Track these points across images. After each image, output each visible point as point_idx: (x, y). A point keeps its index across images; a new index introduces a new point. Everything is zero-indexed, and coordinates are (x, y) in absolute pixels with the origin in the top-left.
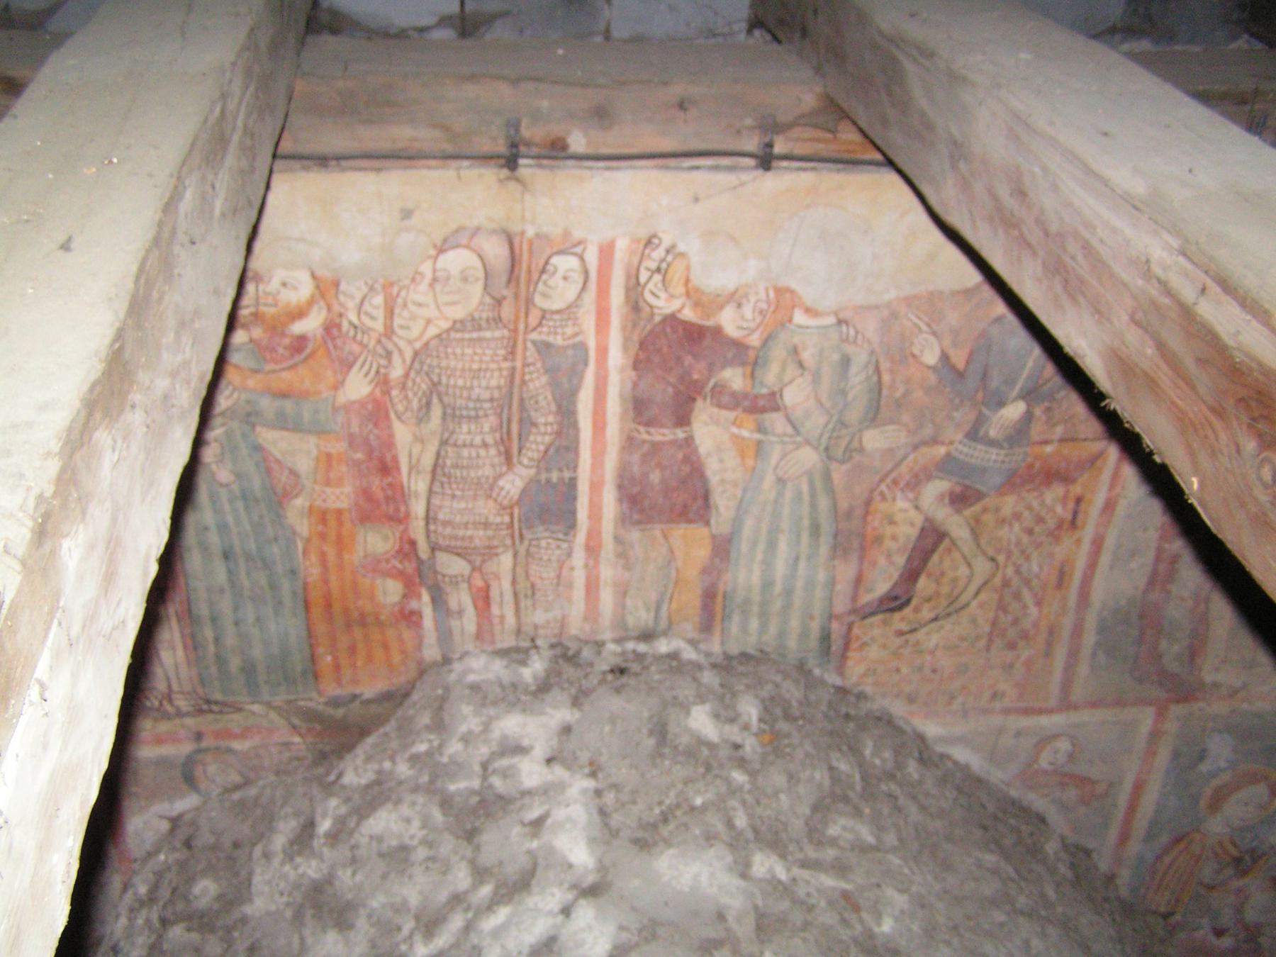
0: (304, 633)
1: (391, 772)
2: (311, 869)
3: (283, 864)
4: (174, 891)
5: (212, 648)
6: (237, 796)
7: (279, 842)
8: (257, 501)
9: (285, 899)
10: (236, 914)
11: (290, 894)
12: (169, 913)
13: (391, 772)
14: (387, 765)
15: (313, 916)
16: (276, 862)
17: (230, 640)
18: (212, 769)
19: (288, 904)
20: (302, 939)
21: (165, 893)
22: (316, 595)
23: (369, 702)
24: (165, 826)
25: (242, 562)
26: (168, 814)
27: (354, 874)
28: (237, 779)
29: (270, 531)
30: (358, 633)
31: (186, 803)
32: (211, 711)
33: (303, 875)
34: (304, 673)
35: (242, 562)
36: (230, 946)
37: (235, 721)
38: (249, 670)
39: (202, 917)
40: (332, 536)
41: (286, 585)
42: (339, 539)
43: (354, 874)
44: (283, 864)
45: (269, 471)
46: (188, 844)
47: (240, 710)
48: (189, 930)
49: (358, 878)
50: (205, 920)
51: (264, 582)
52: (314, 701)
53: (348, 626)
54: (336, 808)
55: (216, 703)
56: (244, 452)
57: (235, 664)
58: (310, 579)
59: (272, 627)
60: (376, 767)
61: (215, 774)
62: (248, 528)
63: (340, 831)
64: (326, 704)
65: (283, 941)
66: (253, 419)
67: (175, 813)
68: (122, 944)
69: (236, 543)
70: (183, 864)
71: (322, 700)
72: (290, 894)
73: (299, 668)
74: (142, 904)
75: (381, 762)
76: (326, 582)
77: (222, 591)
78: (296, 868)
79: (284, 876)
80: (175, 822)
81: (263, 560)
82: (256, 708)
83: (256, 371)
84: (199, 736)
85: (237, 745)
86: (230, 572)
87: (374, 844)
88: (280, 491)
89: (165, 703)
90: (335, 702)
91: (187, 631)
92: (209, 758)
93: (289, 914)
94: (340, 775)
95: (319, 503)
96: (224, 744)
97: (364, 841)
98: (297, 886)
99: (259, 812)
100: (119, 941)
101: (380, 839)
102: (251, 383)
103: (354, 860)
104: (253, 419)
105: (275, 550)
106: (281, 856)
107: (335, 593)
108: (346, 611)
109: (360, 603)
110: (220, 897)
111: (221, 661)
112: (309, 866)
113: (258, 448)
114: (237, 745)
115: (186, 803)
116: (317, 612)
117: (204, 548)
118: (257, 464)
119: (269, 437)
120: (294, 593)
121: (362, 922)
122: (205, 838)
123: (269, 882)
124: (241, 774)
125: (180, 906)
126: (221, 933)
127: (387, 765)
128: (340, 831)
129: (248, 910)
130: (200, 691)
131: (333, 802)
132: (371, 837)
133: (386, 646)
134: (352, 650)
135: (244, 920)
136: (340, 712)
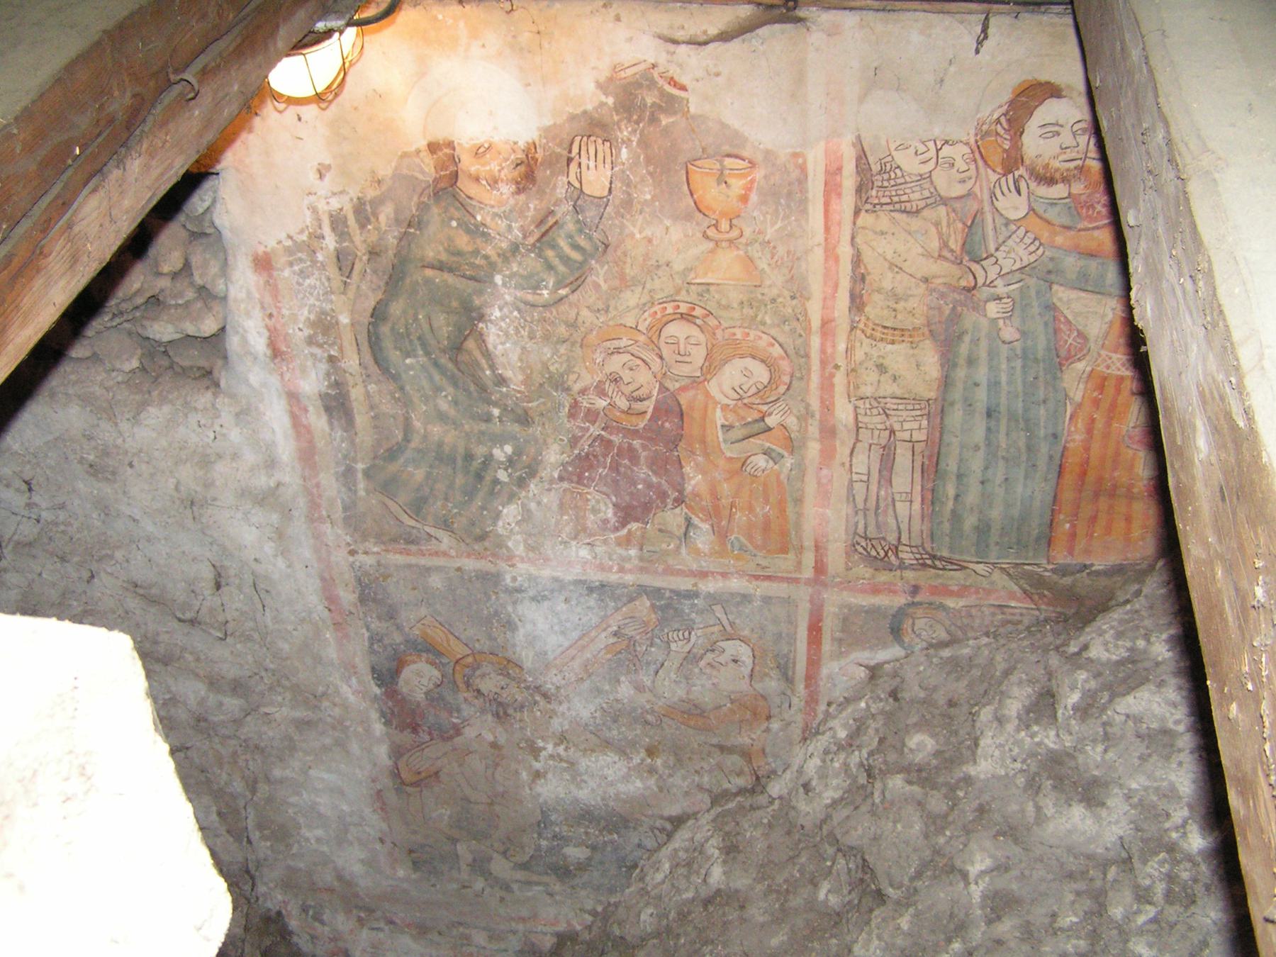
0: (1049, 498)
1: (1145, 651)
2: (1049, 739)
3: (1018, 730)
4: (881, 741)
5: (950, 504)
6: (946, 653)
7: (1013, 707)
8: (1036, 360)
9: (1018, 765)
10: (958, 773)
11: (1024, 761)
12: (878, 761)
13: (1145, 651)
14: (1141, 643)
15: (1054, 787)
16: (1010, 727)
17: (972, 497)
18: (920, 623)
19: (1022, 771)
20: (1038, 809)
21: (870, 740)
22: (1073, 461)
23: (1098, 573)
24: (862, 673)
25: (1004, 422)
26: (866, 662)
27: (1106, 751)
28: (943, 635)
29: (1041, 394)
30: (1103, 503)
31: (888, 654)
32: (935, 567)
33: (1039, 744)
34: (1038, 540)
35: (1004, 422)
36: (955, 805)
37: (955, 578)
38: (983, 530)
39: (920, 771)
40: (1105, 405)
41: (1044, 449)
42: (1113, 406)
43: (1106, 751)
44: (1018, 730)
45: (1056, 331)
46: (894, 695)
47: (963, 568)
48: (910, 783)
49: (1110, 755)
50: (924, 774)
51: (1022, 443)
52: (1043, 568)
53: (1097, 495)
54: (1086, 681)
55: (941, 559)
56: (1036, 310)
57: (970, 521)
58: (1071, 445)
59: (1020, 489)
60: (1129, 644)
61: (923, 628)
62: (1020, 389)
63: (1090, 706)
64: (1053, 571)
65: (1014, 807)
66: (1053, 277)
67: (872, 663)
68: (814, 783)
69: (1003, 400)
70: (889, 716)
71: (1051, 567)
72: (1024, 761)
73: (1035, 533)
74: (840, 748)
75: (1134, 639)
76: (1087, 449)
77: (977, 448)
78: (1032, 737)
79: (1018, 743)
80: (874, 672)
81: (1027, 421)
82: (980, 568)
83: (1068, 228)
84: (915, 590)
85: (951, 603)
86: (989, 429)
87: (1131, 723)
88: (1063, 353)
89: (890, 553)
90: (1063, 571)
91: (930, 485)
92: (920, 612)
93: (1021, 781)
94: (1085, 647)
95: (1101, 368)
96: (937, 600)
97: (1119, 719)
98: (1032, 755)
99: (976, 672)
100: (810, 780)
101: (1138, 720)
102: (1059, 240)
103: (1106, 737)
104: (1053, 277)
105: (1042, 411)
106: (1016, 722)
107: (1094, 461)
108: (1100, 480)
109: (1116, 474)
110: (937, 754)
111: (956, 517)
112: (1047, 737)
113: (1051, 307)
114: (951, 603)
115: (888, 654)
116: (1069, 479)
117: (969, 404)
118: (1046, 324)
119: (1062, 295)
120: (1051, 457)
121: (1116, 801)
122: (913, 691)
123: (1001, 745)
124: (948, 632)
125: (892, 757)
126: (944, 790)
127: (1141, 643)
128: (1090, 706)
129: (972, 770)
130: (928, 546)
131: (1082, 676)
132: (1128, 716)
133: (1128, 519)
134: (1094, 519)
135: (968, 780)
136: (1067, 581)
